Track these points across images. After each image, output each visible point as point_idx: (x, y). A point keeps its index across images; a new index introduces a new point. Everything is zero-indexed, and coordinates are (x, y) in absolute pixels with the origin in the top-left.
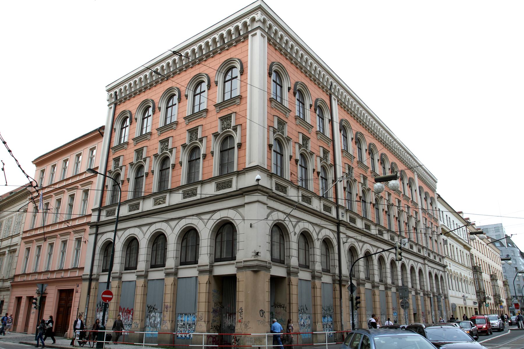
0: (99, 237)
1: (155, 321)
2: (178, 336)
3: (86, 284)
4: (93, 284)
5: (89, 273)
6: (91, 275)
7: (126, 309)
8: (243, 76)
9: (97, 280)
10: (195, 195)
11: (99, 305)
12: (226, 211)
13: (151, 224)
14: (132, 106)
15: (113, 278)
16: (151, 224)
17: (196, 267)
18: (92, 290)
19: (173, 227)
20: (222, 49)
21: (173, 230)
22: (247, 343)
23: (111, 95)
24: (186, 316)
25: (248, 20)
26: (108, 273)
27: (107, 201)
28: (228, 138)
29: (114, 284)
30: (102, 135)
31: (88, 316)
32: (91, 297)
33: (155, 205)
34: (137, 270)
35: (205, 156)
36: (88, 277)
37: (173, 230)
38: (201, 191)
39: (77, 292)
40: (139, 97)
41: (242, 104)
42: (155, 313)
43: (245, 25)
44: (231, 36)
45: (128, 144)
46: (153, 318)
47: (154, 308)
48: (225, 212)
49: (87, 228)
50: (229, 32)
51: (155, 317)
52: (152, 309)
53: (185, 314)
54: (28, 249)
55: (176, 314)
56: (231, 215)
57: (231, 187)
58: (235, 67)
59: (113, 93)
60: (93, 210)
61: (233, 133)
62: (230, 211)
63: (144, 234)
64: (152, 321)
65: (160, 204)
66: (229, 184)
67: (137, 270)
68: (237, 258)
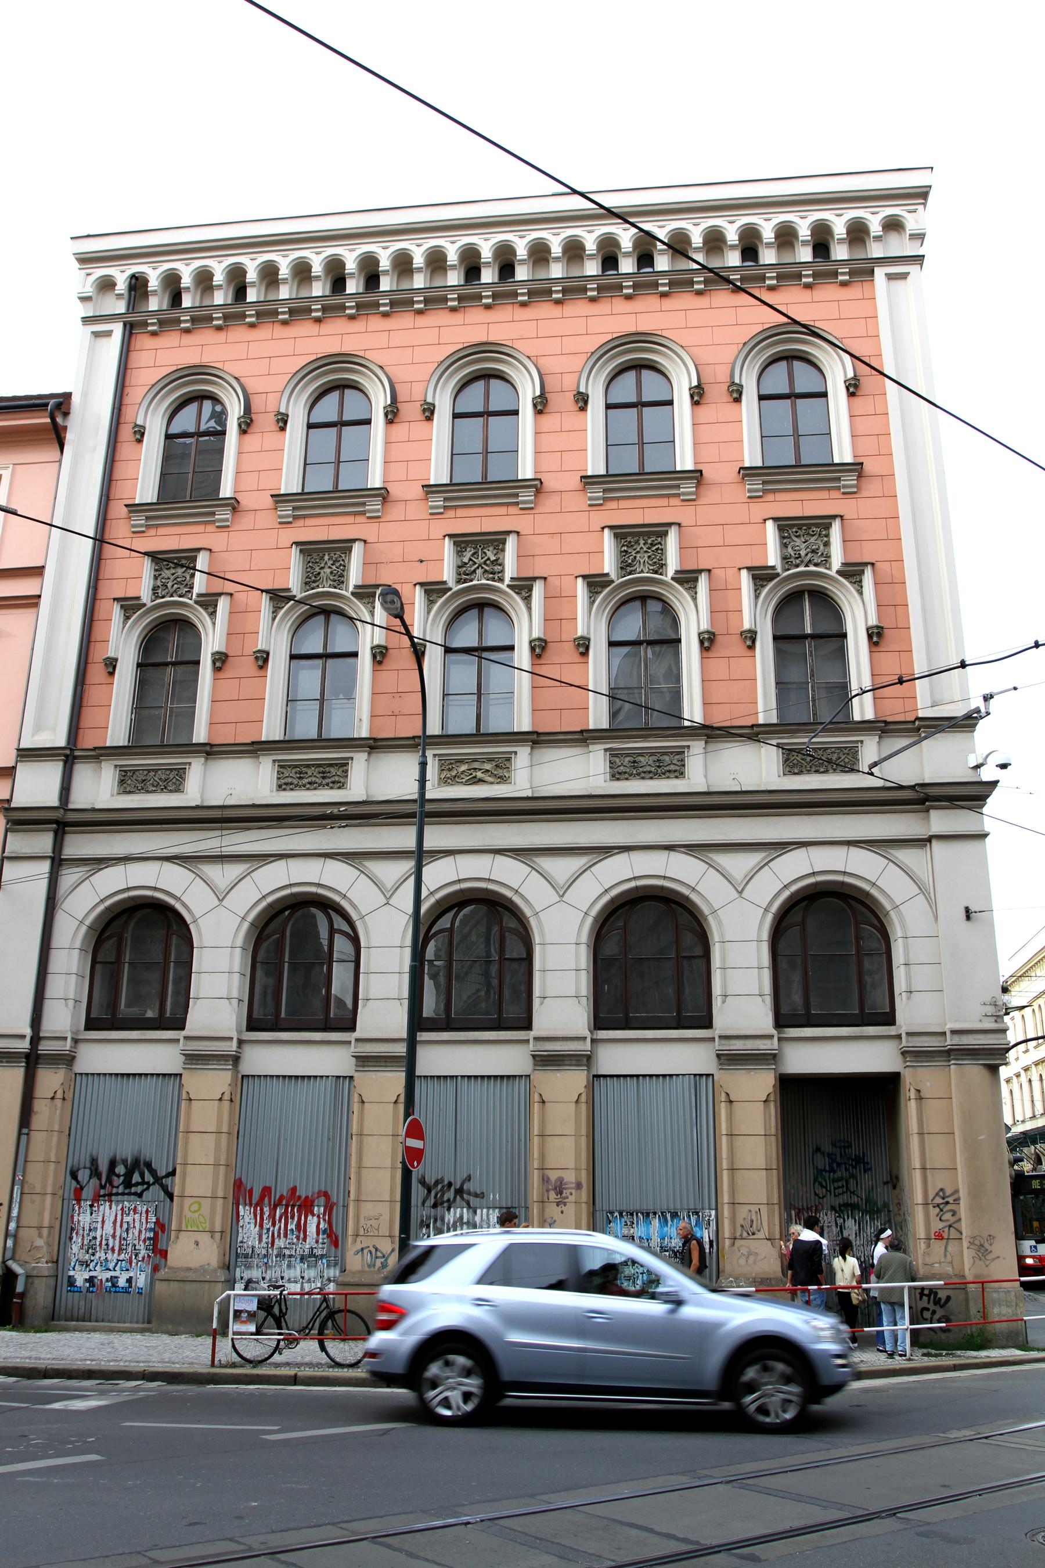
0: (69, 877)
2: (71, 1281)
4: (50, 1080)
7: (283, 1189)
8: (247, 437)
9: (68, 1060)
10: (178, 789)
11: (83, 1175)
13: (606, 851)
16: (606, 851)
21: (562, 891)
22: (996, 1310)
24: (656, 1222)
27: (116, 724)
32: (38, 1139)
35: (221, 660)
36: (25, 1045)
37: (562, 891)
40: (620, 305)
41: (864, 494)
43: (858, 233)
47: (460, 1192)
50: (204, 279)
53: (647, 1215)
56: (681, 872)
59: (121, 277)
60: (27, 754)
61: (200, 617)
67: (356, 1034)
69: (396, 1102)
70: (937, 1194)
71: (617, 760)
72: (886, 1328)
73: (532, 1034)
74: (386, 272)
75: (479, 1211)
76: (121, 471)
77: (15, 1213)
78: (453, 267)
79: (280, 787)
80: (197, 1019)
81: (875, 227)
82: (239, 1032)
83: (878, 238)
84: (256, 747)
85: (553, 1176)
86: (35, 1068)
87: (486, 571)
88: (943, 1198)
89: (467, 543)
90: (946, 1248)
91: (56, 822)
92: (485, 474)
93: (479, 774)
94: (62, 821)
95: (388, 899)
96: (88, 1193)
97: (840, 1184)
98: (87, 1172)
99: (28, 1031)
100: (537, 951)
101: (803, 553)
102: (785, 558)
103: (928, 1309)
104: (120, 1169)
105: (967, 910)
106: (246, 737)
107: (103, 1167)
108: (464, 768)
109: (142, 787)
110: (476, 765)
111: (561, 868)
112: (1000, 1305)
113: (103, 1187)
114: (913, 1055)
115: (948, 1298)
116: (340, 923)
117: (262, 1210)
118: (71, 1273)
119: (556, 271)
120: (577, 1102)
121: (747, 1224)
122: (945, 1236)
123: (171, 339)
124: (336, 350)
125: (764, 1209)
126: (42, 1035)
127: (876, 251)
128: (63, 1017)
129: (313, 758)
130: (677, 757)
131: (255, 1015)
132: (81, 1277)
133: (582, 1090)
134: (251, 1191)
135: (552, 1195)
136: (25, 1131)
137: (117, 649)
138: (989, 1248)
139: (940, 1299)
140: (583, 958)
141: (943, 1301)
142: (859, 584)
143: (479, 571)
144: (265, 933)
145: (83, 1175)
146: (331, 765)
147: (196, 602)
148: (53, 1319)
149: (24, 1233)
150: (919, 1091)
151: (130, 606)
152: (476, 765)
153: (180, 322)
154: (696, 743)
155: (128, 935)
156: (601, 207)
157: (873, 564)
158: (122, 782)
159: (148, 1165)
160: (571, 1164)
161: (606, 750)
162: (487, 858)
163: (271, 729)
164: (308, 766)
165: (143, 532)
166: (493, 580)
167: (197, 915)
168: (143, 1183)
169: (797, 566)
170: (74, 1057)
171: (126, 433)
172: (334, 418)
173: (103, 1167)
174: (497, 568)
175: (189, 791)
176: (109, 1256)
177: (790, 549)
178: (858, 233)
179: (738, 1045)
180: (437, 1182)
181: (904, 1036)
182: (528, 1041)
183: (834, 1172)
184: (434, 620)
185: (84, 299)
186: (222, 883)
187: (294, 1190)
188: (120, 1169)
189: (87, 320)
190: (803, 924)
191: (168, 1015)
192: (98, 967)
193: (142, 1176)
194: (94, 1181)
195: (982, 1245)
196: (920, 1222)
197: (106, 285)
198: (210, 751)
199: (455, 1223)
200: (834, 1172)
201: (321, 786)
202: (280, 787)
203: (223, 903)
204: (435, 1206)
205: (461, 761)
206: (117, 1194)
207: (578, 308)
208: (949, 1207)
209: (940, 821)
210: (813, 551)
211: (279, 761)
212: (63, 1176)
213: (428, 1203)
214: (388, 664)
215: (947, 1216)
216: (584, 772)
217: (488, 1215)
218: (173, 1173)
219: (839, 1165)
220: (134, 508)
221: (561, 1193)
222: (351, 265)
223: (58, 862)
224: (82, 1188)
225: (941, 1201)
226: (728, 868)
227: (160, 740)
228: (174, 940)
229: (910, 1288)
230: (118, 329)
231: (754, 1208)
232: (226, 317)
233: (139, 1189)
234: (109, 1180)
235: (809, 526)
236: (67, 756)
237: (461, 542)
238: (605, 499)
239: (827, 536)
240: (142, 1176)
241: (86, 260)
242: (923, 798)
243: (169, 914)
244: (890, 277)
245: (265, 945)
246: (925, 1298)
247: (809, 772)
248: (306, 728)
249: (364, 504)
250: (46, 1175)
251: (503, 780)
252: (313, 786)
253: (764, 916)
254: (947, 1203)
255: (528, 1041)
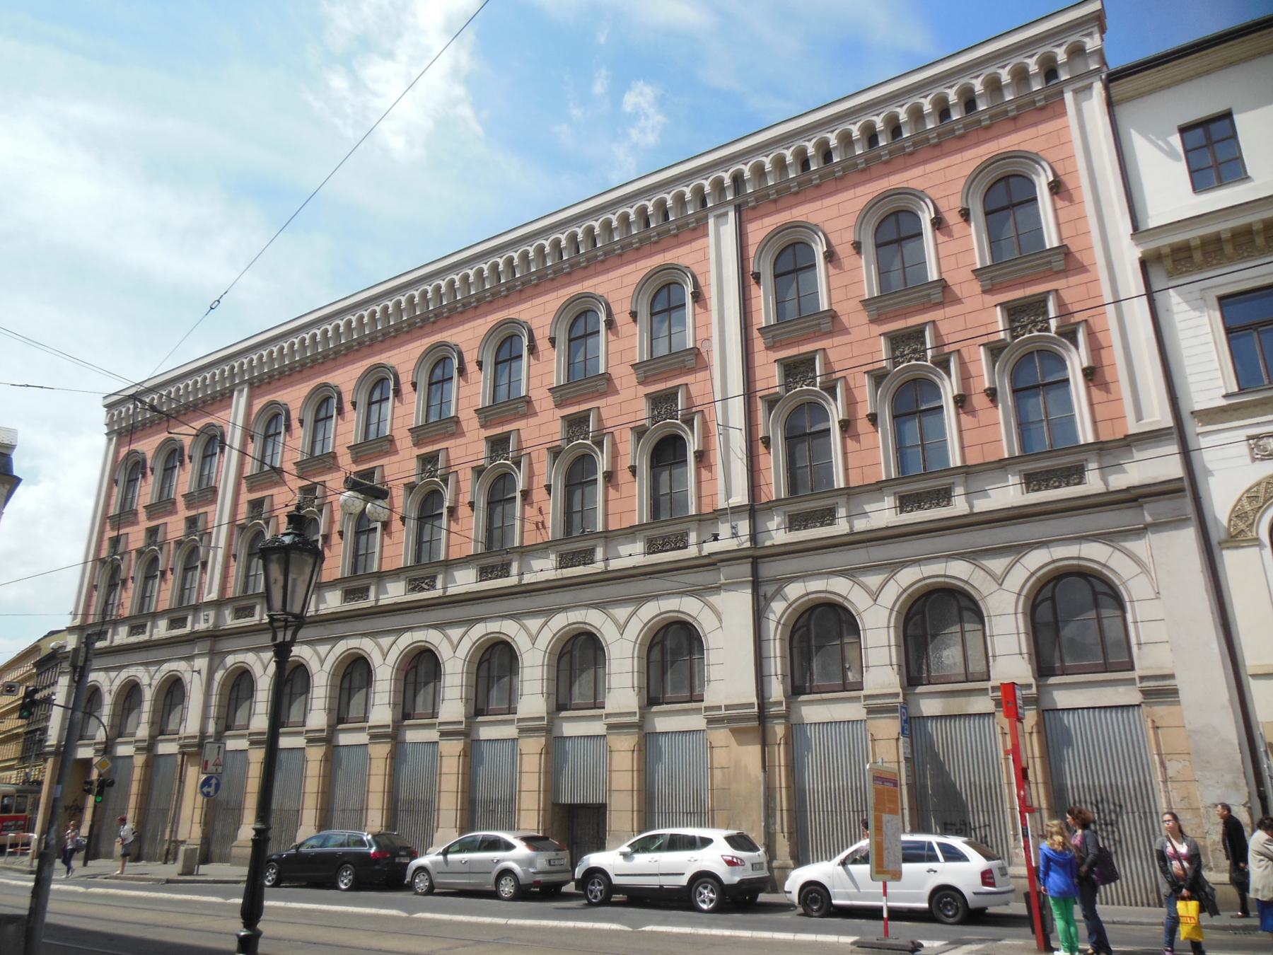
5: (963, 671)
14: (148, 446)
19: (455, 642)
21: (875, 596)
23: (113, 415)
27: (774, 483)
28: (193, 551)
37: (455, 648)
38: (1153, 437)
44: (544, 261)
50: (680, 198)
63: (455, 648)
65: (422, 590)
67: (517, 716)
73: (703, 704)
79: (413, 590)
99: (754, 700)
116: (1100, 587)
172: (894, 237)
223: (756, 585)
243: (840, 610)
245: (911, 623)
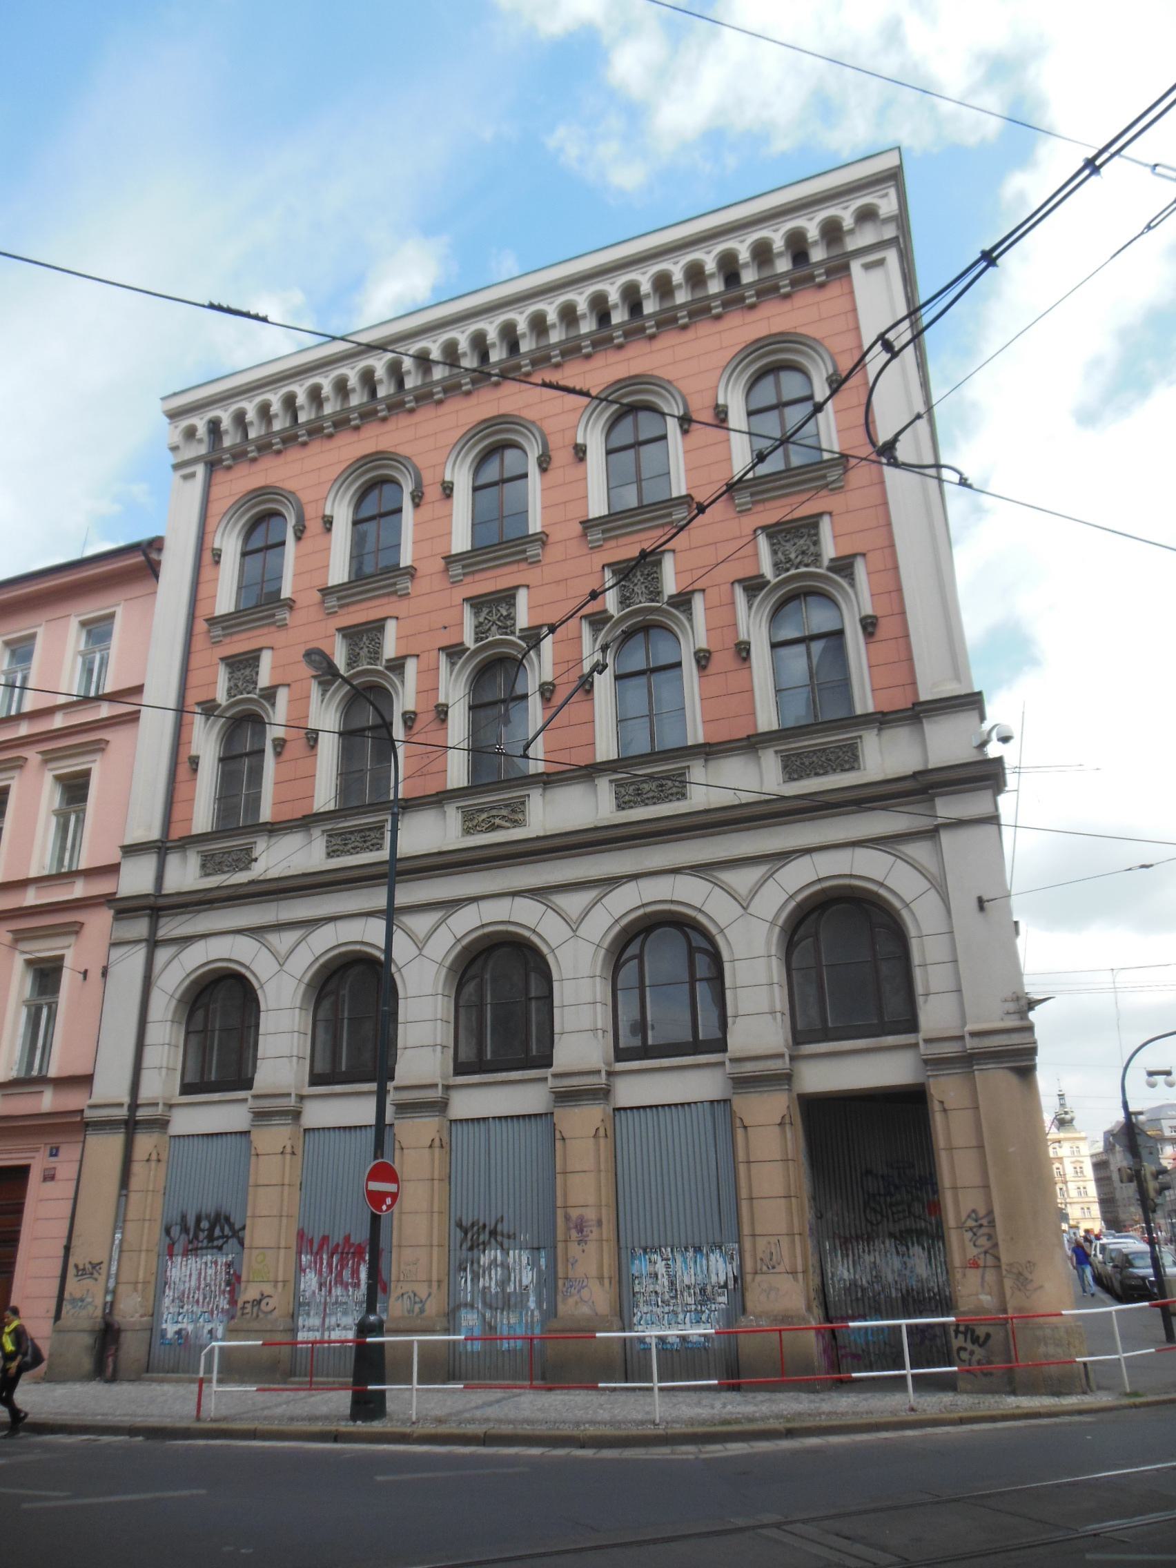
1: (503, 1283)
2: (163, 1333)
3: (115, 1141)
6: (134, 1106)
7: (337, 1238)
8: (302, 542)
9: (161, 1124)
11: (175, 1231)
12: (229, 939)
13: (784, 857)
15: (402, 1108)
16: (784, 857)
17: (245, 1100)
18: (137, 1168)
20: (367, 415)
21: (574, 926)
25: (846, 213)
26: (373, 1086)
27: (202, 817)
29: (415, 1134)
30: (152, 570)
31: (123, 1278)
33: (467, 831)
34: (556, 1068)
37: (574, 926)
39: (49, 1177)
42: (506, 1252)
43: (832, 232)
45: (291, 608)
46: (497, 1274)
47: (493, 1233)
48: (493, 904)
49: (99, 922)
51: (505, 1266)
52: (484, 1237)
54: (46, 975)
55: (623, 1253)
56: (525, 915)
57: (852, 769)
58: (278, 514)
59: (200, 423)
60: (131, 850)
62: (860, 852)
64: (490, 1282)
65: (494, 828)
66: (245, 859)
68: (256, 1084)
69: (431, 1146)
70: (969, 1216)
71: (622, 790)
72: (908, 1372)
74: (647, 296)
75: (511, 1252)
76: (204, 591)
77: (114, 1269)
78: (780, 254)
79: (620, 807)
80: (742, 1038)
81: (848, 222)
82: (608, 1064)
83: (851, 231)
84: (441, 796)
85: (574, 1213)
86: (134, 1133)
87: (500, 627)
88: (976, 1221)
89: (482, 603)
90: (983, 1278)
91: (151, 908)
92: (640, 498)
93: (497, 821)
94: (155, 907)
95: (420, 950)
96: (178, 1248)
97: (900, 1208)
98: (178, 1228)
100: (915, 945)
101: (793, 556)
102: (776, 565)
103: (965, 1349)
104: (205, 1224)
105: (981, 901)
106: (432, 787)
107: (191, 1222)
108: (484, 816)
109: (641, 799)
110: (494, 812)
111: (573, 903)
112: (1046, 1344)
113: (191, 1242)
114: (743, 1083)
115: (988, 1336)
117: (321, 1259)
118: (164, 1326)
119: (681, 297)
120: (595, 1136)
121: (767, 1260)
122: (981, 1263)
123: (242, 470)
124: (372, 449)
125: (785, 1242)
126: (139, 1102)
127: (852, 244)
128: (160, 1083)
129: (649, 770)
130: (632, 788)
131: (622, 1045)
132: (171, 1329)
133: (599, 1124)
134: (311, 1241)
135: (574, 1234)
136: (124, 1192)
137: (447, 695)
138: (1030, 1277)
139: (978, 1337)
140: (776, 970)
141: (981, 1340)
142: (850, 577)
143: (494, 628)
144: (796, 938)
145: (175, 1231)
146: (370, 829)
147: (261, 696)
148: (147, 1371)
149: (122, 1289)
150: (942, 1102)
151: (209, 708)
152: (494, 812)
153: (323, 428)
154: (535, 791)
155: (488, 976)
156: (359, 344)
157: (864, 555)
158: (203, 866)
159: (227, 1219)
160: (591, 1200)
161: (611, 781)
162: (506, 902)
163: (606, 749)
164: (351, 833)
165: (749, 509)
166: (506, 634)
167: (263, 980)
168: (222, 1237)
169: (788, 570)
170: (609, 1091)
171: (207, 557)
172: (774, 401)
173: (191, 1222)
174: (509, 623)
175: (868, 767)
176: (195, 1309)
177: (780, 554)
178: (832, 232)
179: (749, 1068)
180: (473, 1225)
181: (921, 1043)
182: (545, 1079)
183: (892, 1195)
184: (756, 612)
185: (174, 449)
186: (574, 913)
187: (347, 1239)
188: (205, 1224)
189: (176, 467)
190: (640, 957)
191: (489, 1057)
192: (462, 1011)
193: (222, 1230)
194: (183, 1236)
195: (1020, 1274)
196: (960, 1246)
197: (190, 433)
198: (547, 781)
199: (490, 1265)
200: (892, 1195)
201: (363, 849)
202: (620, 807)
203: (750, 910)
204: (471, 1249)
205: (482, 811)
206: (202, 1248)
207: (704, 329)
208: (984, 1230)
209: (947, 808)
210: (803, 553)
211: (781, 751)
212: (158, 1230)
213: (464, 1247)
214: (712, 668)
215: (982, 1241)
216: (760, 778)
217: (520, 1256)
218: (244, 1228)
219: (896, 1187)
220: (213, 621)
221: (581, 1231)
222: (614, 297)
223: (153, 944)
224: (173, 1244)
225: (974, 1224)
226: (734, 886)
227: (238, 823)
228: (533, 976)
229: (908, 1326)
230: (200, 470)
231: (773, 1240)
232: (793, 283)
233: (220, 1242)
234: (196, 1237)
235: (247, 660)
236: (159, 848)
237: (477, 603)
238: (605, 540)
239: (817, 534)
240: (222, 1230)
241: (173, 415)
242: (924, 786)
244: (867, 267)
246: (961, 1337)
247: (808, 776)
248: (641, 746)
249: (395, 584)
250: (145, 1230)
251: (517, 823)
252: (356, 850)
253: (770, 930)
254: (981, 1226)
255: (545, 1079)
